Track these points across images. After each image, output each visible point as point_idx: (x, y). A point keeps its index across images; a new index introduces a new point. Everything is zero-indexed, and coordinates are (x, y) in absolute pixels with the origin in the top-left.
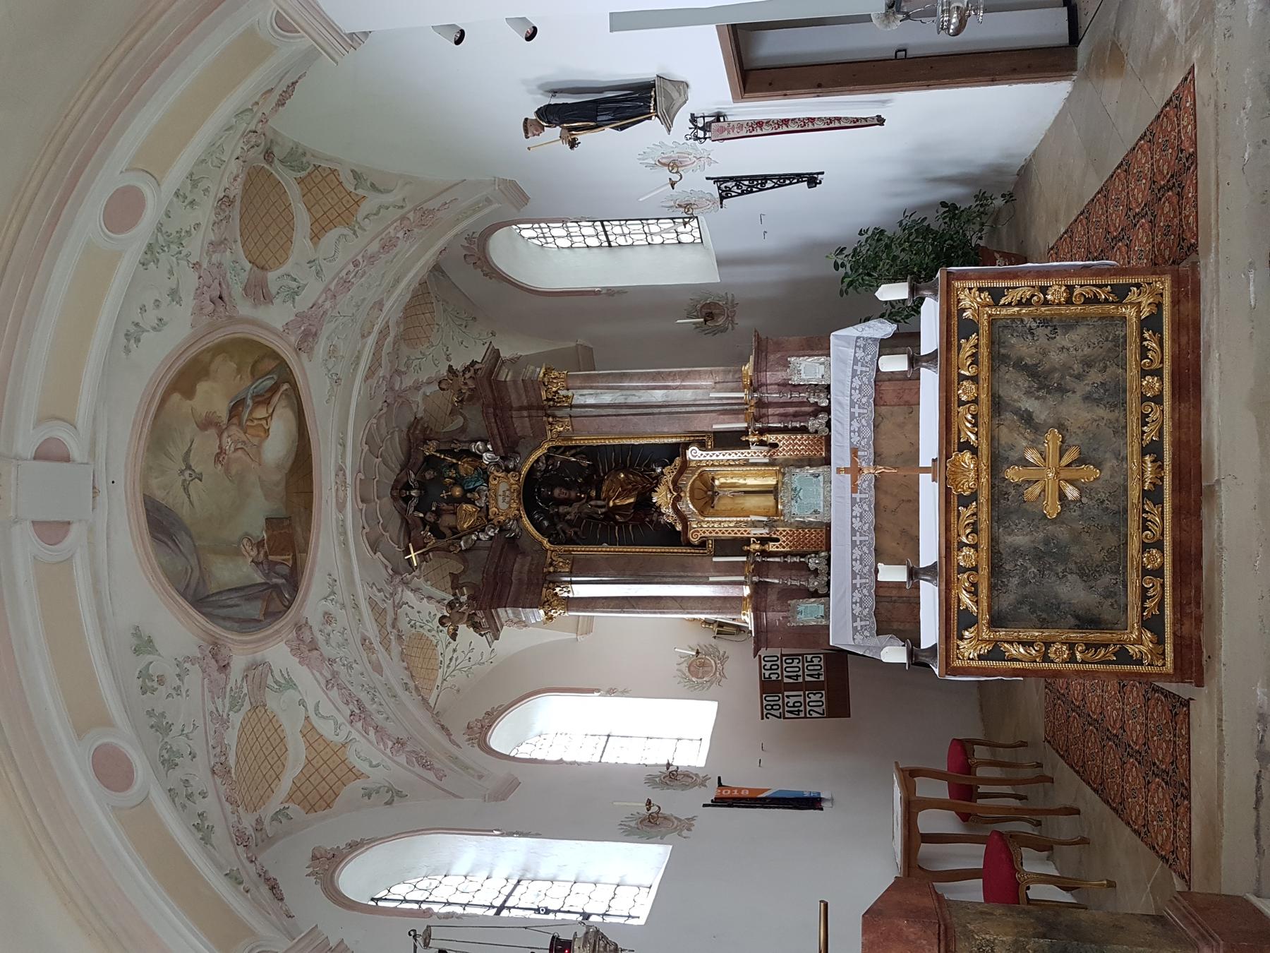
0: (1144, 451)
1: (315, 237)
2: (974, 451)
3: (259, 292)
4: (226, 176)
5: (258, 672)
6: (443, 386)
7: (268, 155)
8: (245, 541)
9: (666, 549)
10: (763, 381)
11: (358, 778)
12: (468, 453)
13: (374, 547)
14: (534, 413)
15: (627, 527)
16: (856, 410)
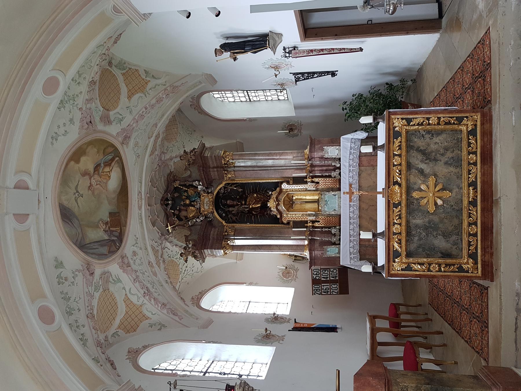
0: (469, 185)
1: (129, 97)
2: (400, 185)
3: (106, 120)
4: (93, 72)
5: (106, 276)
6: (182, 158)
7: (110, 64)
8: (100, 222)
9: (273, 225)
10: (313, 156)
11: (147, 319)
12: (192, 186)
13: (154, 224)
14: (219, 169)
15: (257, 216)
16: (351, 168)
